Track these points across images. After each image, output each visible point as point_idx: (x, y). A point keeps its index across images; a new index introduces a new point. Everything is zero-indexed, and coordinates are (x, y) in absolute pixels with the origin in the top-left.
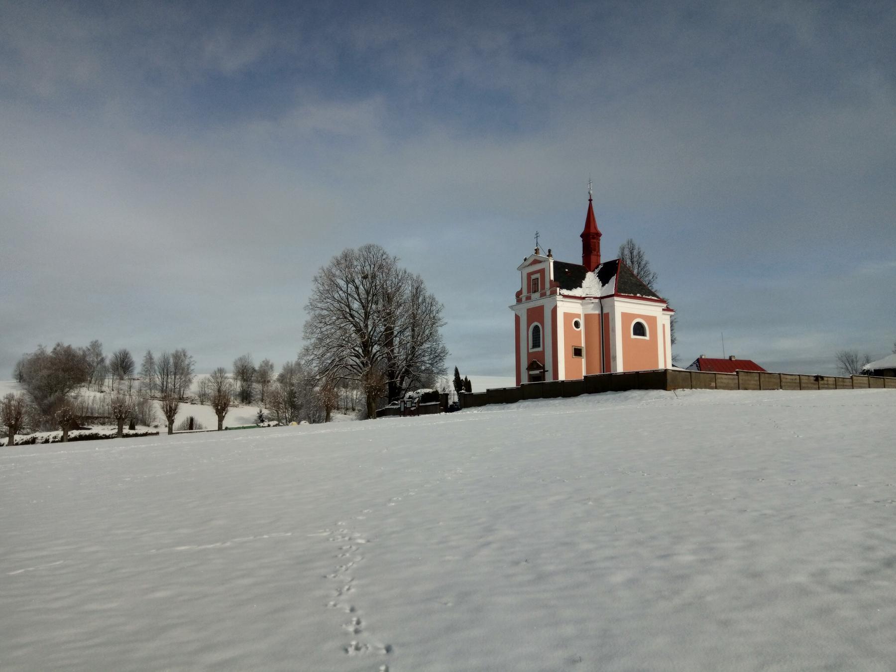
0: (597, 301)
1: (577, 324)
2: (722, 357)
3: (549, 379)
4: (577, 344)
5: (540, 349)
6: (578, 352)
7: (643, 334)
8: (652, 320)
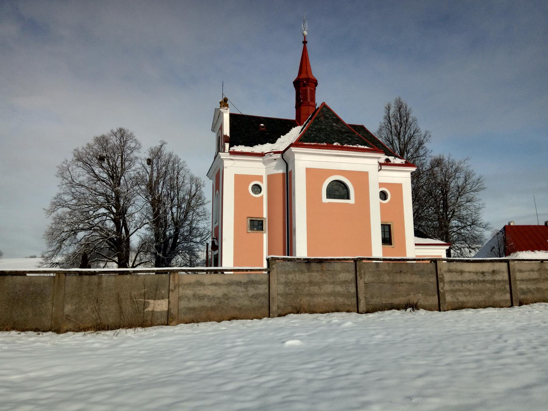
0: (279, 156)
1: (257, 188)
2: (536, 224)
4: (255, 215)
6: (257, 225)
7: (331, 194)
8: (362, 178)
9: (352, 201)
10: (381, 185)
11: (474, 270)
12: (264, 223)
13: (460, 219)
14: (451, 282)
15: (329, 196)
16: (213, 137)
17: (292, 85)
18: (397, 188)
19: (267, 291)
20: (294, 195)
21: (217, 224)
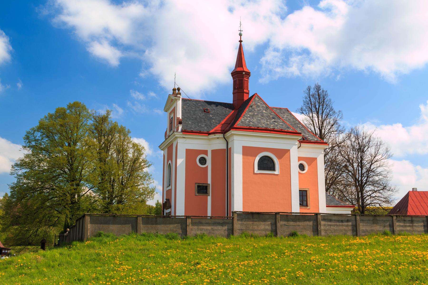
1: (203, 161)
3: (173, 214)
4: (201, 182)
5: (170, 188)
9: (276, 172)
10: (300, 159)
11: (337, 219)
12: (208, 188)
13: (374, 183)
14: (325, 225)
15: (260, 168)
16: (165, 117)
17: (231, 75)
18: (312, 161)
19: (232, 227)
20: (233, 167)
21: (170, 188)
